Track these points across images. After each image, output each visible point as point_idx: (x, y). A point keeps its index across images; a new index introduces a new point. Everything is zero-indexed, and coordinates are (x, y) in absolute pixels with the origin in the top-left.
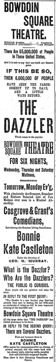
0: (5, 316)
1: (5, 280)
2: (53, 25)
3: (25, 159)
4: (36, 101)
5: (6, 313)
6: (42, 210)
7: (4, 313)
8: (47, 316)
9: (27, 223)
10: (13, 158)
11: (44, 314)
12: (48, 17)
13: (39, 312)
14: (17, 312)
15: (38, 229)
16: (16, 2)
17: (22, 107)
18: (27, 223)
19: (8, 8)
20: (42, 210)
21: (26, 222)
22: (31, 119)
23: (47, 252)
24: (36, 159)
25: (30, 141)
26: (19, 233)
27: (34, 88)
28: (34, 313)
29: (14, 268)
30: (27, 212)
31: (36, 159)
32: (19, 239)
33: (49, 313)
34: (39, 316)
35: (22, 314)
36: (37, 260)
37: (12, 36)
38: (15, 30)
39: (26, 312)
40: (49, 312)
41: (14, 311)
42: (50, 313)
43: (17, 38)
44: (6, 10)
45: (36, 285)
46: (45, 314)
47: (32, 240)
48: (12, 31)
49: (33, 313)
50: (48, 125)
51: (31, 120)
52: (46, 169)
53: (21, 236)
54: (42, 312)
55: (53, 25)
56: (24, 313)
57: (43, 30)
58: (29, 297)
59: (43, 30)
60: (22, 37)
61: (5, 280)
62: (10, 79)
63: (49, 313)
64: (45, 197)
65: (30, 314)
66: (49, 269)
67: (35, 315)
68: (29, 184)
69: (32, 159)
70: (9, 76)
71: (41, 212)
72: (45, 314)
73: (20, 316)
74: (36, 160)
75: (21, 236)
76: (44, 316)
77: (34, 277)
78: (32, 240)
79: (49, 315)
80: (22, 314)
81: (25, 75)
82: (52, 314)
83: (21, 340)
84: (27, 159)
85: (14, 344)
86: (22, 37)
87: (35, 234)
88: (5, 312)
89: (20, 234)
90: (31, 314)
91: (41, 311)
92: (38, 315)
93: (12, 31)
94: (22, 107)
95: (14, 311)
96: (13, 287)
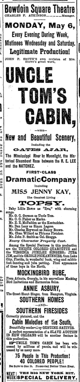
1: (26, 45)
2: (43, 80)
5: (8, 8)
6: (43, 8)
8: (66, 12)
10: (21, 308)
11: (63, 9)
13: (42, 355)
14: (23, 6)
16: (3, 183)
18: (63, 11)
20: (43, 8)
23: (10, 79)
24: (37, 271)
27: (32, 343)
28: (47, 8)
29: (31, 160)
31: (37, 271)
32: (32, 139)
33: (69, 8)
34: (55, 12)
35: (30, 9)
36: (71, 377)
38: (28, 308)
39: (36, 7)
40: (69, 6)
42: (70, 8)
43: (29, 313)
44: (7, 11)
45: (29, 361)
46: (64, 9)
49: (46, 7)
50: (39, 299)
52: (63, 42)
54: (58, 6)
55: (43, 80)
56: (34, 8)
57: (37, 286)
58: (46, 312)
59: (37, 286)
61: (26, 45)
62: (41, 362)
63: (69, 8)
65: (42, 9)
66: (65, 150)
67: (50, 11)
68: (28, 320)
69: (33, 275)
70: (33, 309)
71: (43, 10)
72: (64, 9)
73: (28, 12)
74: (37, 272)
75: (8, 8)
76: (63, 12)
77: (42, 34)
79: (69, 12)
80: (30, 9)
81: (26, 349)
82: (74, 9)
83: (47, 376)
86: (59, 301)
88: (7, 7)
89: (8, 7)
90: (44, 9)
91: (58, 5)
93: (21, 92)
95: (19, 5)
96: (37, 290)
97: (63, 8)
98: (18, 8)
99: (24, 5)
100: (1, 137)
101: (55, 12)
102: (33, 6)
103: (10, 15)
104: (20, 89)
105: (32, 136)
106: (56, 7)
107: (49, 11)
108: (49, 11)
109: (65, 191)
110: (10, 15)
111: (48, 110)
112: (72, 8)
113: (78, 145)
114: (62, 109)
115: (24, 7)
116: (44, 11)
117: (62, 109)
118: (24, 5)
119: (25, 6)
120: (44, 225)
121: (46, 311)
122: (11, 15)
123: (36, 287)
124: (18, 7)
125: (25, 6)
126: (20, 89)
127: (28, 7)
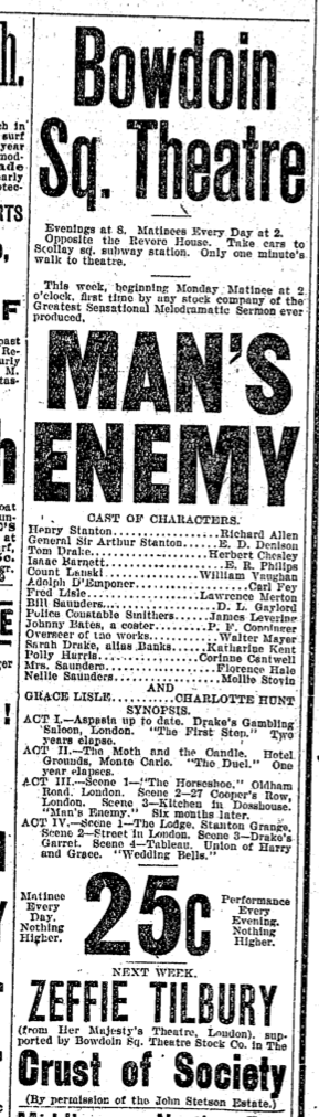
0: (96, 100)
3: (263, 988)
4: (124, 984)
7: (81, 65)
9: (300, 185)
12: (220, 196)
14: (236, 49)
15: (29, 909)
17: (158, 1003)
19: (99, 77)
21: (292, 179)
22: (114, 1020)
25: (269, 695)
26: (90, 41)
28: (276, 155)
30: (292, 179)
33: (258, 153)
34: (141, 194)
37: (32, 1001)
40: (260, 137)
41: (199, 36)
42: (269, 147)
44: (89, 92)
47: (227, 988)
48: (154, 989)
51: (114, 1016)
52: (250, 141)
53: (106, 65)
54: (171, 136)
60: (115, 1010)
63: (258, 153)
64: (146, 1066)
73: (271, 106)
75: (106, 65)
78: (227, 988)
84: (274, 989)
85: (242, 291)
86: (115, 1010)
87: (237, 1066)
89: (100, 56)
92: (82, 1017)
93: (154, 989)
94: (158, 1003)
97: (206, 154)
98: (191, 61)
99: (244, 38)
100: (67, 1115)
101: (141, 194)
102: (54, 134)
103: (193, 698)
104: (152, 985)
105: (90, 54)
106: (153, 136)
107: (292, 190)
108: (292, 190)
109: (256, 1021)
110: (193, 698)
111: (89, 498)
112: (285, 157)
113: (311, 910)
114: (79, 425)
115: (243, 54)
116: (226, 187)
117: (79, 425)
118: (244, 38)
119: (251, 47)
120: (61, 590)
121: (77, 1001)
122: (198, 697)
123: (122, 992)
124: (186, 53)
125: (251, 47)
126: (152, 985)
127: (271, 56)
